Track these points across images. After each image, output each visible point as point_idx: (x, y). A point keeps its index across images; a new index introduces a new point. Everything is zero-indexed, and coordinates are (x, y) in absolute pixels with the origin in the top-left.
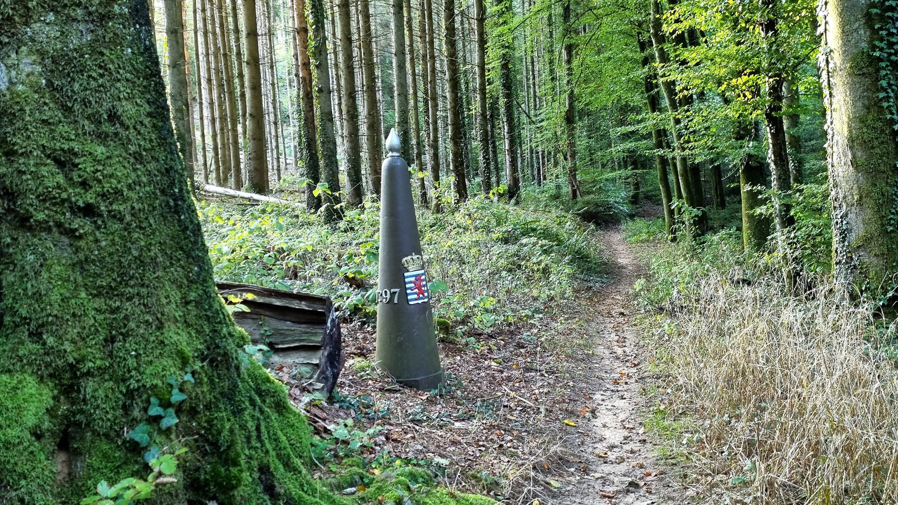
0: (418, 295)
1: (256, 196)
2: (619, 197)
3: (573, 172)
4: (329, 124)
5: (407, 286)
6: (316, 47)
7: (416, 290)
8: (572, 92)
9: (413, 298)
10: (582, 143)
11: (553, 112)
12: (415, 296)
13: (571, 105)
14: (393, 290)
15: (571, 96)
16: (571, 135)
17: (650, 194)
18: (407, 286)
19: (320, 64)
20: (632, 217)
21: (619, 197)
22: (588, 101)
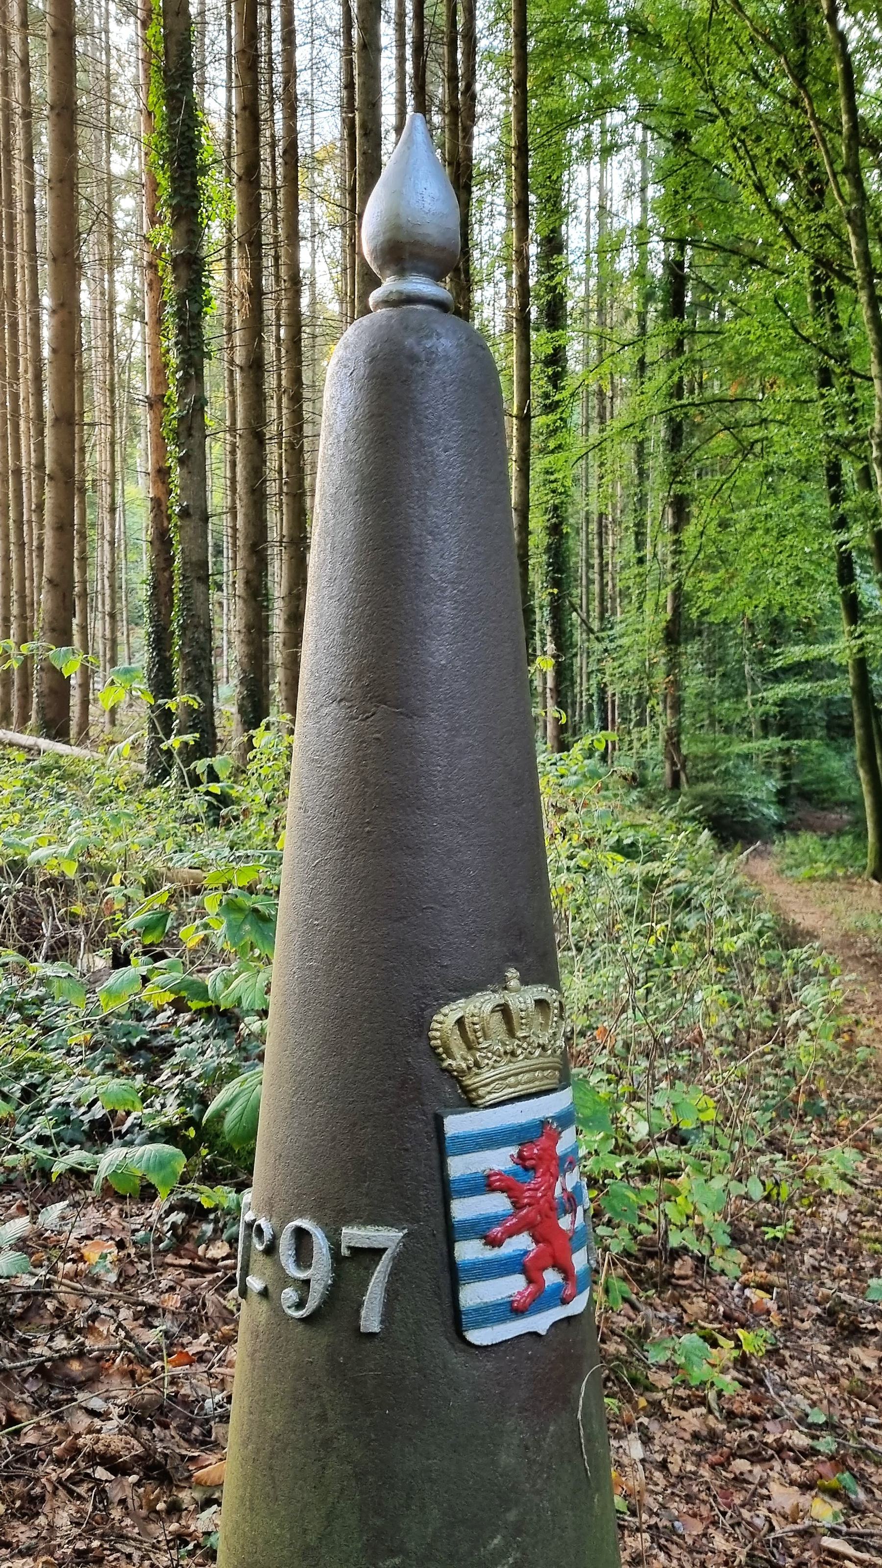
0: (532, 1275)
1: (44, 743)
2: (760, 790)
4: (198, 588)
5: (463, 1209)
6: (181, 419)
7: (522, 1243)
8: (680, 585)
9: (497, 1302)
11: (638, 629)
12: (514, 1286)
13: (676, 609)
14: (355, 1235)
15: (679, 594)
16: (673, 665)
17: (807, 788)
18: (463, 1209)
19: (188, 455)
20: (779, 827)
21: (760, 790)
22: (706, 605)
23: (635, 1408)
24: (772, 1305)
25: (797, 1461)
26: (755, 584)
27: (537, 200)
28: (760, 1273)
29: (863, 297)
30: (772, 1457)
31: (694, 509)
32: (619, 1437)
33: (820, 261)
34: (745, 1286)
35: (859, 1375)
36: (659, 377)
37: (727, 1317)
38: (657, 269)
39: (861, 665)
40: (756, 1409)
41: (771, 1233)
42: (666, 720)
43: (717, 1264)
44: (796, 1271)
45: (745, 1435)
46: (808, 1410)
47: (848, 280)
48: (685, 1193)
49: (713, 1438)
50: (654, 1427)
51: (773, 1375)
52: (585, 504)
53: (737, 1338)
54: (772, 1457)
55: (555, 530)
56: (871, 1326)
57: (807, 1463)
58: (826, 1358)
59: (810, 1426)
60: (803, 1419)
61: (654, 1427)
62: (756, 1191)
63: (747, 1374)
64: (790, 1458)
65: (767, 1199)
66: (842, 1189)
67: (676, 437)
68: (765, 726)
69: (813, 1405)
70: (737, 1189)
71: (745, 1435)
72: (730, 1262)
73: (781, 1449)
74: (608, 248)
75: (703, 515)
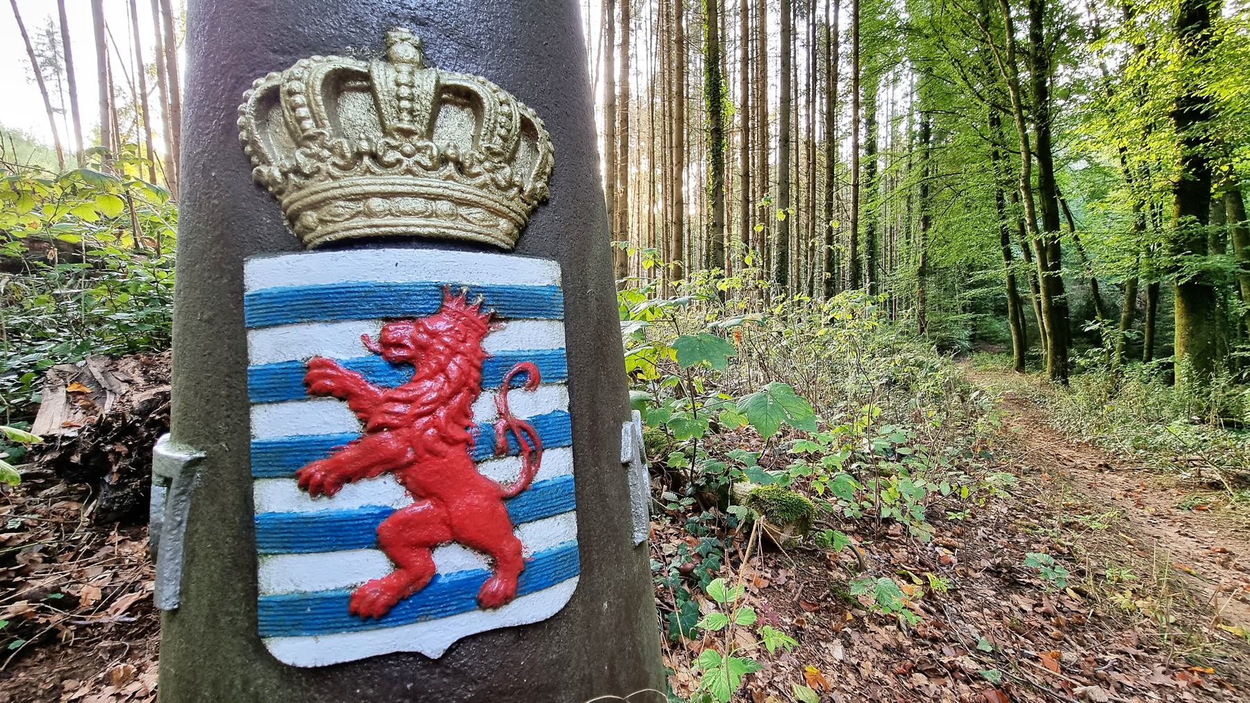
0: (397, 538)
3: (922, 315)
4: (719, 252)
7: (382, 493)
10: (932, 291)
12: (366, 568)
16: (922, 284)
23: (844, 620)
24: (954, 560)
25: (967, 682)
26: (960, 251)
27: (867, 105)
28: (947, 537)
29: (1016, 117)
30: (946, 674)
31: (933, 221)
32: (827, 641)
33: (995, 106)
34: (936, 545)
35: (1018, 616)
36: (917, 169)
37: (922, 563)
38: (917, 128)
39: (1012, 279)
40: (937, 633)
41: (952, 516)
42: (918, 307)
43: (914, 531)
44: (972, 539)
45: (926, 653)
46: (978, 637)
47: (1008, 112)
48: (894, 486)
49: (900, 650)
50: (855, 637)
51: (952, 608)
52: (884, 223)
53: (926, 578)
54: (946, 674)
55: (870, 233)
56: (1027, 581)
57: (976, 686)
58: (992, 600)
59: (978, 652)
60: (973, 646)
61: (855, 637)
62: (946, 490)
63: (932, 605)
64: (961, 679)
65: (955, 496)
66: (1003, 495)
67: (925, 191)
68: (964, 309)
69: (982, 634)
70: (933, 487)
71: (926, 653)
72: (924, 532)
73: (954, 669)
74: (896, 120)
75: (937, 224)
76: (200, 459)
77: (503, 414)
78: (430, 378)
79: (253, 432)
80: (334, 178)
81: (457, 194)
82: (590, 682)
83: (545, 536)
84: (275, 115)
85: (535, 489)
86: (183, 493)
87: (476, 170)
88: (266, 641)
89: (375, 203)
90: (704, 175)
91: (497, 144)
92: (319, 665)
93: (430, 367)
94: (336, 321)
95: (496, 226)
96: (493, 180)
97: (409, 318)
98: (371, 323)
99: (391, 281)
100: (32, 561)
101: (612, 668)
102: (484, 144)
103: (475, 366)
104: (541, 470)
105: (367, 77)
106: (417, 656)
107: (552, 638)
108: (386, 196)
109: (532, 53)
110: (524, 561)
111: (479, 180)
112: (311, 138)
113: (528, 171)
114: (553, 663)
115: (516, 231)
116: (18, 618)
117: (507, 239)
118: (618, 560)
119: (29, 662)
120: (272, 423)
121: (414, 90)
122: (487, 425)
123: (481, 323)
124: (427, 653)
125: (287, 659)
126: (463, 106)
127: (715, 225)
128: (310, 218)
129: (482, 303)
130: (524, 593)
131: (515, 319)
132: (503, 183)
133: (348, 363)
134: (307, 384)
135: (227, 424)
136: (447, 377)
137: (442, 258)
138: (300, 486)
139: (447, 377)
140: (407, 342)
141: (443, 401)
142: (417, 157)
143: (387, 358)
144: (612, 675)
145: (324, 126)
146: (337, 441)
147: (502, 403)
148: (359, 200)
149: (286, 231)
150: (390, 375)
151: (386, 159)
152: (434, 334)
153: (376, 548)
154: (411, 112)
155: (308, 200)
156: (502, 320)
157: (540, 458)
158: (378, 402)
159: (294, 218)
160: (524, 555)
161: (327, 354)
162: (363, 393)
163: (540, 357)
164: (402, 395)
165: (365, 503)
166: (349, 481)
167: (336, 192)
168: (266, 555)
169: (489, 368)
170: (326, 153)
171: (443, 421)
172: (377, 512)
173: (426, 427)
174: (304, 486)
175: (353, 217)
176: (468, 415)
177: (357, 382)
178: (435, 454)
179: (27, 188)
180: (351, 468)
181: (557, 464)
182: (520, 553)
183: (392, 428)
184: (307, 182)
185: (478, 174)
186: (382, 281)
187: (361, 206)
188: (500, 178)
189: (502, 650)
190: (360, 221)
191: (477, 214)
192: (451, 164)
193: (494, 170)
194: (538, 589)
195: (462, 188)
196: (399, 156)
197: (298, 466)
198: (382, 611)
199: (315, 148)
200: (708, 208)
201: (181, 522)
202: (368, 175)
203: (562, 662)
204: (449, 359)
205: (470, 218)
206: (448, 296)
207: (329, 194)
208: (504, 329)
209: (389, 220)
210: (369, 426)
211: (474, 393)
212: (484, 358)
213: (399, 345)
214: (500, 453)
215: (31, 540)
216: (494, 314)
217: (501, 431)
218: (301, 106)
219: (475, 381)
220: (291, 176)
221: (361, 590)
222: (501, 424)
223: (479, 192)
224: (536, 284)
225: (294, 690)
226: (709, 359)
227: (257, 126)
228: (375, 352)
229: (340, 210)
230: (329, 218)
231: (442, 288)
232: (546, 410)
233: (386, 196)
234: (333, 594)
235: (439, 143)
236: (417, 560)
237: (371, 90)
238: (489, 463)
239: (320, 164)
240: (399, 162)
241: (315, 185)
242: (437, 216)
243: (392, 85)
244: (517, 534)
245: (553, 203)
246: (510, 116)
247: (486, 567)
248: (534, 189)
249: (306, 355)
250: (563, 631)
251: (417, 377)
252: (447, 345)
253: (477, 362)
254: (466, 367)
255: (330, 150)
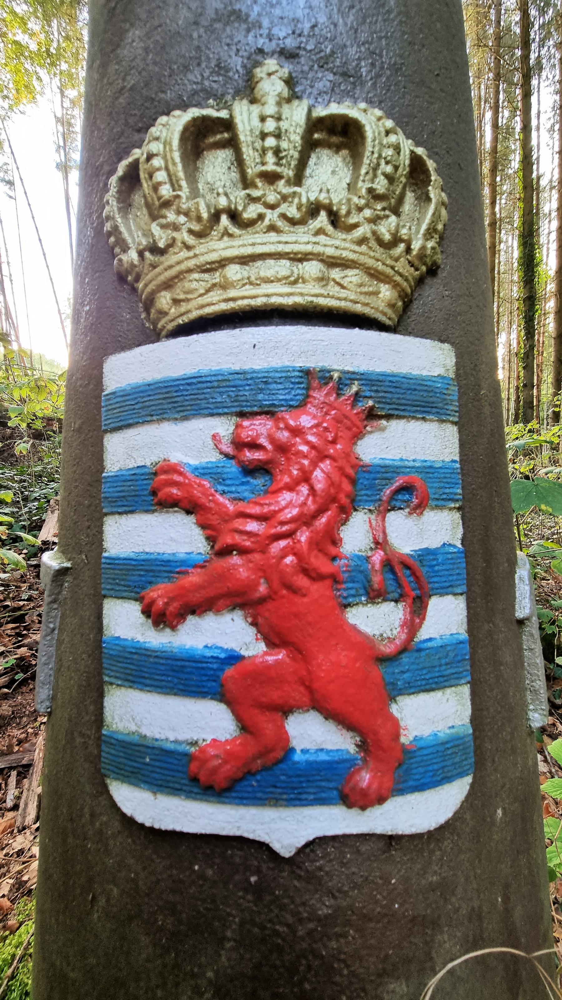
4: (529, 411)
7: (226, 633)
12: (206, 723)
76: (67, 569)
77: (380, 543)
78: (290, 488)
79: (106, 545)
80: (188, 248)
81: (330, 251)
82: (480, 918)
83: (432, 715)
84: (137, 199)
85: (419, 650)
86: (54, 601)
87: (353, 220)
88: (108, 781)
89: (234, 272)
90: (514, 344)
91: (381, 185)
92: (157, 826)
93: (290, 475)
94: (186, 418)
95: (376, 293)
96: (374, 233)
97: (267, 413)
98: (223, 419)
99: (247, 367)
100: (33, 621)
101: (506, 899)
102: (363, 187)
103: (348, 476)
104: (426, 623)
105: (228, 125)
106: (263, 847)
107: (432, 852)
108: (245, 260)
109: (422, 83)
110: (406, 751)
111: (358, 233)
112: (167, 204)
113: (417, 224)
114: (432, 888)
115: (400, 304)
116: (21, 659)
117: (389, 312)
118: (514, 751)
119: (24, 689)
120: (129, 536)
121: (281, 123)
122: (359, 557)
123: (354, 419)
124: (276, 846)
125: (127, 809)
126: (337, 148)
127: (525, 386)
128: (164, 300)
129: (357, 394)
130: (401, 792)
131: (399, 417)
132: (387, 237)
133: (196, 469)
134: (154, 493)
135: (88, 536)
136: (312, 490)
137: (309, 336)
138: (143, 612)
139: (312, 490)
140: (263, 441)
141: (305, 520)
142: (283, 208)
143: (240, 463)
144: (507, 910)
145: (180, 188)
146: (183, 562)
147: (380, 529)
148: (215, 270)
149: (143, 325)
150: (243, 484)
151: (245, 216)
152: (297, 432)
153: (221, 701)
154: (277, 151)
155: (162, 278)
156: (381, 417)
157: (426, 607)
158: (228, 518)
159: (149, 303)
160: (403, 740)
161: (175, 457)
162: (212, 505)
163: (428, 470)
164: (256, 510)
165: (210, 642)
166: (193, 612)
167: (191, 264)
168: (111, 684)
169: (363, 481)
170: (182, 219)
171: (305, 547)
172: (223, 656)
173: (285, 553)
174: (147, 612)
175: (208, 291)
176: (336, 542)
177: (206, 493)
178: (294, 590)
179: (43, 384)
180: (196, 597)
181: (446, 618)
182: (397, 736)
183: (243, 551)
184: (162, 259)
185: (356, 226)
186: (237, 367)
187: (216, 277)
188: (385, 230)
189: (369, 859)
190: (215, 296)
191: (353, 277)
192: (323, 214)
193: (375, 220)
194: (420, 788)
195: (335, 244)
196: (260, 209)
197: (143, 588)
198: (224, 784)
199: (171, 216)
200: (518, 367)
201: (54, 630)
202: (226, 238)
203: (444, 889)
204: (314, 465)
205: (345, 282)
206: (315, 383)
207: (183, 267)
208: (383, 429)
209: (249, 291)
210: (217, 547)
211: (345, 512)
212: (359, 466)
213: (254, 446)
214: (375, 596)
215: (34, 608)
216: (372, 408)
217: (377, 567)
218: (158, 169)
219: (348, 496)
220: (147, 254)
221: (203, 750)
222: (378, 557)
223: (357, 248)
224: (425, 373)
225: (133, 841)
226: (547, 504)
227: (120, 209)
228: (227, 456)
229: (194, 285)
230: (182, 296)
231: (307, 373)
232: (434, 543)
233: (245, 260)
234: (172, 747)
235: (310, 191)
236: (265, 722)
237: (233, 143)
238: (360, 608)
239: (175, 234)
240: (261, 217)
241: (171, 259)
242: (304, 282)
243: (256, 122)
244: (394, 709)
245: (442, 274)
246: (397, 149)
247: (352, 749)
248: (423, 248)
249: (154, 459)
250: (447, 844)
251: (274, 488)
252: (312, 446)
253: (351, 472)
254: (336, 477)
255: (186, 214)
